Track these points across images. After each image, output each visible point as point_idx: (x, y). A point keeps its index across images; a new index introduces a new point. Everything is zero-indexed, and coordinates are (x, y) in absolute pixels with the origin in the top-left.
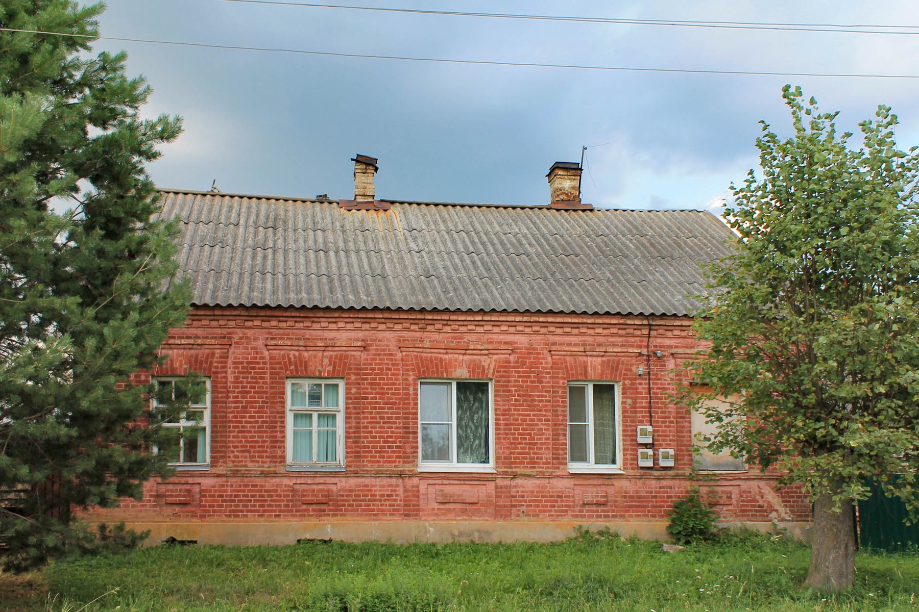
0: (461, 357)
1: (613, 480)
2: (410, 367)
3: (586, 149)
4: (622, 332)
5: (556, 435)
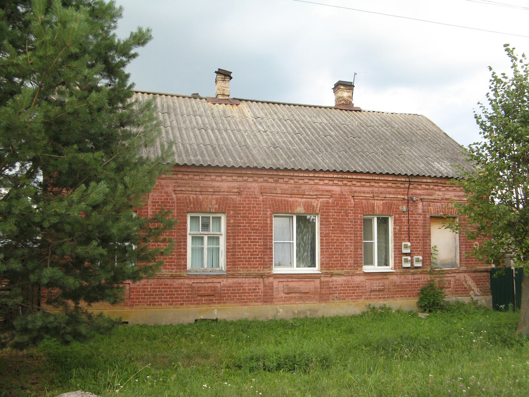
0: (300, 200)
1: (388, 276)
2: (268, 206)
3: (356, 74)
4: (394, 185)
5: (356, 249)
